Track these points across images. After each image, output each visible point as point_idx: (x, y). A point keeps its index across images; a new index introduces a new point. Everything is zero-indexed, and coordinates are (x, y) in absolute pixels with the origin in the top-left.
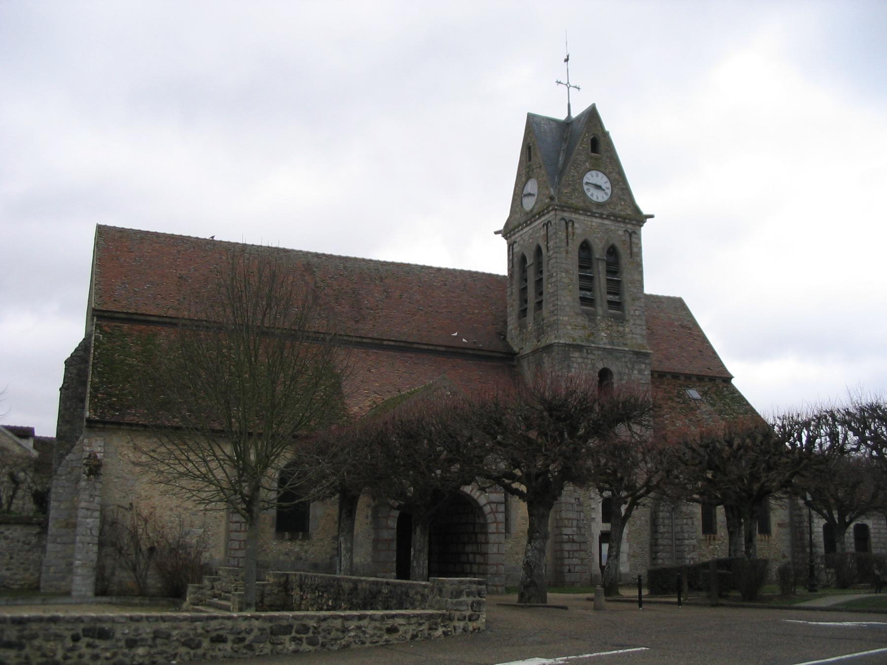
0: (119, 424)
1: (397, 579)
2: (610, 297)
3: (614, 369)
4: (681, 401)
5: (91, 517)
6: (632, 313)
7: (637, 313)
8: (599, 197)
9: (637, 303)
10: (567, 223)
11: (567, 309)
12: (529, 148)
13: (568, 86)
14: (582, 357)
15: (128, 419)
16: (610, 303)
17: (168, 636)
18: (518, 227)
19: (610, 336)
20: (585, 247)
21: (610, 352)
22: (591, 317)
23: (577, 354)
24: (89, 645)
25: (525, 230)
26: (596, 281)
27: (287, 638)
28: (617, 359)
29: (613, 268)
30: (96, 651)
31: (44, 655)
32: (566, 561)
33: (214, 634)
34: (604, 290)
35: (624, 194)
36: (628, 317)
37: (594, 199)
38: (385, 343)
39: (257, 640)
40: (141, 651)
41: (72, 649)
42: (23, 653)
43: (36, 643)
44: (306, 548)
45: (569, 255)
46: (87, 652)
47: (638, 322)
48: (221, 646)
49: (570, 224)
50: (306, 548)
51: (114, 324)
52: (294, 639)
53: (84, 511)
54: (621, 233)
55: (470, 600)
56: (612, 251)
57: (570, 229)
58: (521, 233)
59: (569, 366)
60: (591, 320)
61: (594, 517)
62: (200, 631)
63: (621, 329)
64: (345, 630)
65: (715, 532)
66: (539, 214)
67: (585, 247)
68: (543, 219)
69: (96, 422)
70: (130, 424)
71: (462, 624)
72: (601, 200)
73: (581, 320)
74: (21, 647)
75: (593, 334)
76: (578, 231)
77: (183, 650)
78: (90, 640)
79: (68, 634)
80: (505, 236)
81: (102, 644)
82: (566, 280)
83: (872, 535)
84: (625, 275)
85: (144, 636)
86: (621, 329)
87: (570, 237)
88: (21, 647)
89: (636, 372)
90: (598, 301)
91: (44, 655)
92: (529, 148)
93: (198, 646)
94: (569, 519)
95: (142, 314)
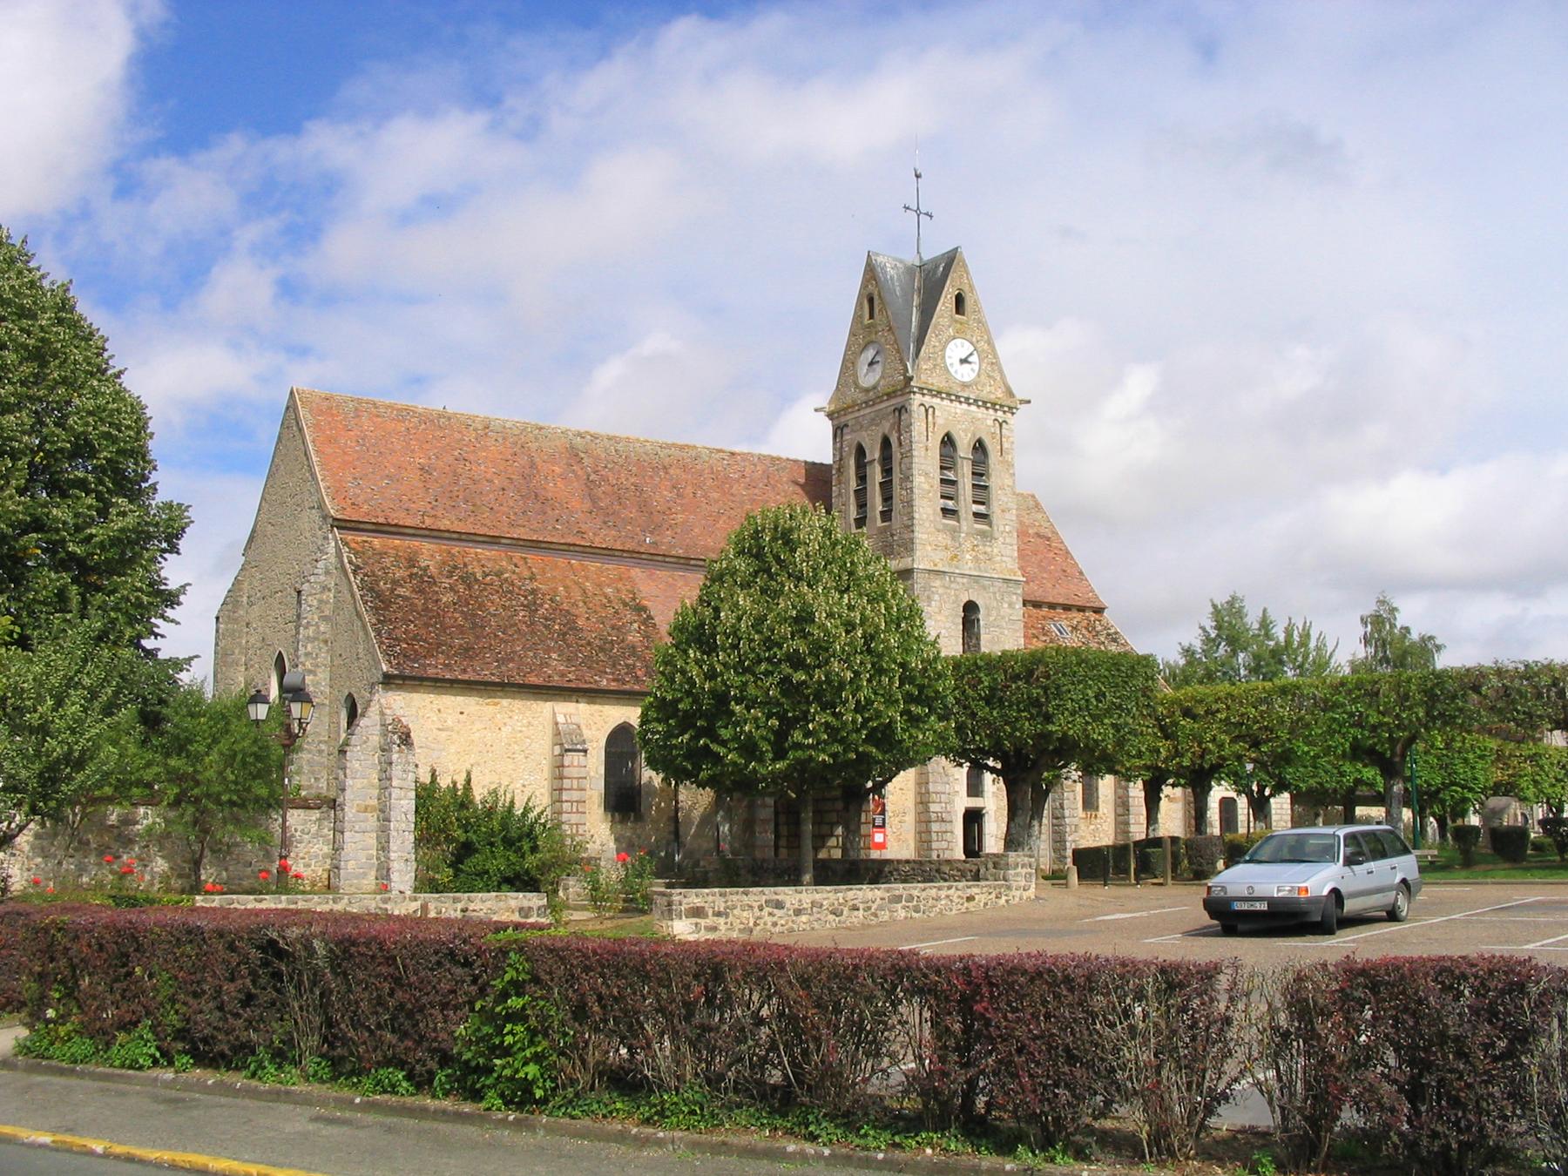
0: (422, 679)
1: (1293, 827)
2: (976, 508)
3: (980, 603)
4: (1048, 639)
5: (405, 797)
6: (1001, 528)
7: (1008, 529)
8: (966, 374)
9: (1007, 516)
10: (927, 411)
11: (927, 524)
12: (871, 301)
13: (918, 212)
14: (944, 586)
15: (431, 672)
16: (976, 515)
17: (822, 905)
18: (853, 407)
19: (976, 559)
20: (948, 441)
21: (976, 579)
22: (954, 532)
23: (938, 583)
24: (770, 914)
25: (862, 413)
26: (960, 485)
27: (899, 906)
28: (984, 588)
29: (979, 470)
30: (775, 919)
31: (742, 923)
32: (934, 845)
33: (851, 903)
34: (970, 499)
35: (993, 371)
36: (996, 535)
37: (958, 377)
38: (692, 562)
39: (880, 908)
40: (804, 918)
41: (759, 918)
42: (729, 920)
43: (735, 912)
44: (638, 831)
45: (929, 453)
46: (769, 920)
47: (1008, 540)
48: (856, 913)
49: (931, 411)
50: (638, 831)
51: (359, 539)
52: (903, 908)
53: (397, 791)
54: (990, 422)
55: (1024, 871)
56: (980, 447)
57: (930, 417)
58: (857, 415)
59: (928, 597)
60: (953, 539)
61: (449, 781)
62: (841, 901)
63: (988, 550)
64: (938, 899)
65: (1097, 809)
66: (888, 394)
67: (948, 441)
68: (893, 401)
69: (395, 677)
70: (436, 680)
71: (1018, 893)
72: (966, 379)
73: (944, 539)
74: (727, 916)
75: (956, 556)
76: (940, 421)
77: (831, 917)
78: (771, 910)
79: (756, 905)
80: (830, 416)
81: (778, 912)
82: (926, 486)
83: (1273, 812)
84: (993, 479)
85: (805, 906)
86: (989, 549)
87: (930, 429)
88: (727, 916)
89: (1006, 605)
90: (962, 514)
91: (742, 923)
92: (871, 301)
93: (841, 914)
94: (936, 793)
95: (396, 525)
